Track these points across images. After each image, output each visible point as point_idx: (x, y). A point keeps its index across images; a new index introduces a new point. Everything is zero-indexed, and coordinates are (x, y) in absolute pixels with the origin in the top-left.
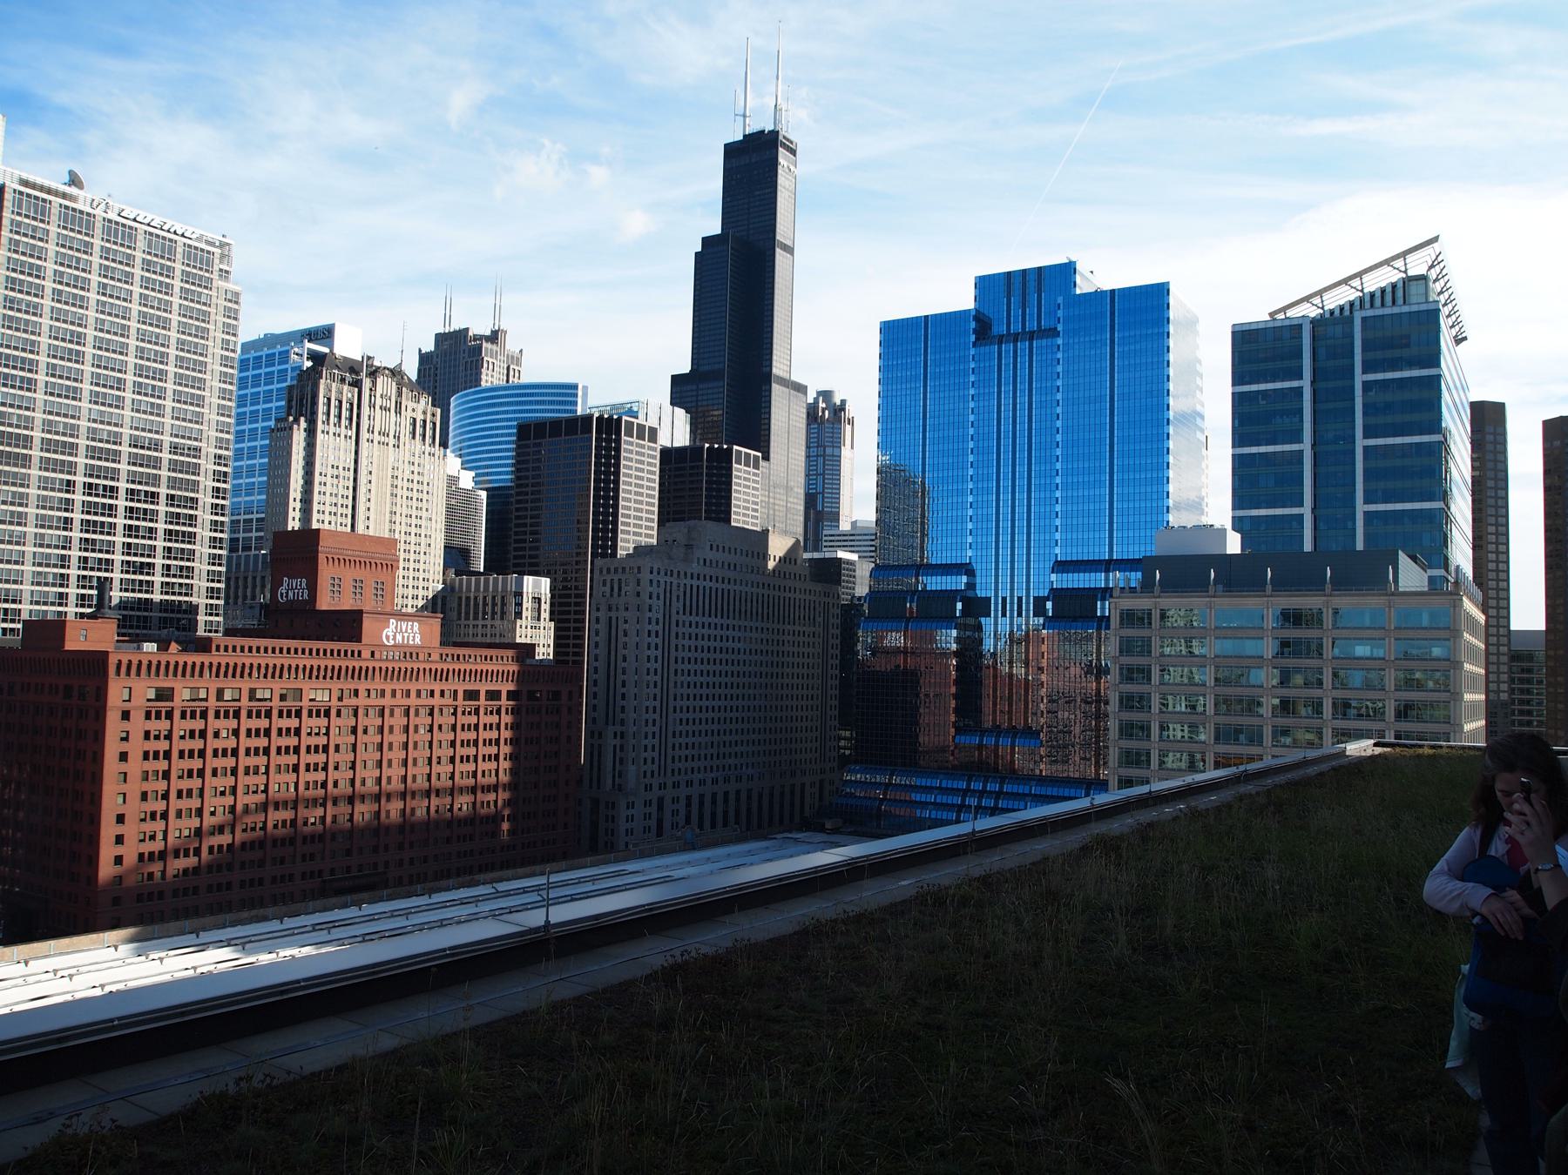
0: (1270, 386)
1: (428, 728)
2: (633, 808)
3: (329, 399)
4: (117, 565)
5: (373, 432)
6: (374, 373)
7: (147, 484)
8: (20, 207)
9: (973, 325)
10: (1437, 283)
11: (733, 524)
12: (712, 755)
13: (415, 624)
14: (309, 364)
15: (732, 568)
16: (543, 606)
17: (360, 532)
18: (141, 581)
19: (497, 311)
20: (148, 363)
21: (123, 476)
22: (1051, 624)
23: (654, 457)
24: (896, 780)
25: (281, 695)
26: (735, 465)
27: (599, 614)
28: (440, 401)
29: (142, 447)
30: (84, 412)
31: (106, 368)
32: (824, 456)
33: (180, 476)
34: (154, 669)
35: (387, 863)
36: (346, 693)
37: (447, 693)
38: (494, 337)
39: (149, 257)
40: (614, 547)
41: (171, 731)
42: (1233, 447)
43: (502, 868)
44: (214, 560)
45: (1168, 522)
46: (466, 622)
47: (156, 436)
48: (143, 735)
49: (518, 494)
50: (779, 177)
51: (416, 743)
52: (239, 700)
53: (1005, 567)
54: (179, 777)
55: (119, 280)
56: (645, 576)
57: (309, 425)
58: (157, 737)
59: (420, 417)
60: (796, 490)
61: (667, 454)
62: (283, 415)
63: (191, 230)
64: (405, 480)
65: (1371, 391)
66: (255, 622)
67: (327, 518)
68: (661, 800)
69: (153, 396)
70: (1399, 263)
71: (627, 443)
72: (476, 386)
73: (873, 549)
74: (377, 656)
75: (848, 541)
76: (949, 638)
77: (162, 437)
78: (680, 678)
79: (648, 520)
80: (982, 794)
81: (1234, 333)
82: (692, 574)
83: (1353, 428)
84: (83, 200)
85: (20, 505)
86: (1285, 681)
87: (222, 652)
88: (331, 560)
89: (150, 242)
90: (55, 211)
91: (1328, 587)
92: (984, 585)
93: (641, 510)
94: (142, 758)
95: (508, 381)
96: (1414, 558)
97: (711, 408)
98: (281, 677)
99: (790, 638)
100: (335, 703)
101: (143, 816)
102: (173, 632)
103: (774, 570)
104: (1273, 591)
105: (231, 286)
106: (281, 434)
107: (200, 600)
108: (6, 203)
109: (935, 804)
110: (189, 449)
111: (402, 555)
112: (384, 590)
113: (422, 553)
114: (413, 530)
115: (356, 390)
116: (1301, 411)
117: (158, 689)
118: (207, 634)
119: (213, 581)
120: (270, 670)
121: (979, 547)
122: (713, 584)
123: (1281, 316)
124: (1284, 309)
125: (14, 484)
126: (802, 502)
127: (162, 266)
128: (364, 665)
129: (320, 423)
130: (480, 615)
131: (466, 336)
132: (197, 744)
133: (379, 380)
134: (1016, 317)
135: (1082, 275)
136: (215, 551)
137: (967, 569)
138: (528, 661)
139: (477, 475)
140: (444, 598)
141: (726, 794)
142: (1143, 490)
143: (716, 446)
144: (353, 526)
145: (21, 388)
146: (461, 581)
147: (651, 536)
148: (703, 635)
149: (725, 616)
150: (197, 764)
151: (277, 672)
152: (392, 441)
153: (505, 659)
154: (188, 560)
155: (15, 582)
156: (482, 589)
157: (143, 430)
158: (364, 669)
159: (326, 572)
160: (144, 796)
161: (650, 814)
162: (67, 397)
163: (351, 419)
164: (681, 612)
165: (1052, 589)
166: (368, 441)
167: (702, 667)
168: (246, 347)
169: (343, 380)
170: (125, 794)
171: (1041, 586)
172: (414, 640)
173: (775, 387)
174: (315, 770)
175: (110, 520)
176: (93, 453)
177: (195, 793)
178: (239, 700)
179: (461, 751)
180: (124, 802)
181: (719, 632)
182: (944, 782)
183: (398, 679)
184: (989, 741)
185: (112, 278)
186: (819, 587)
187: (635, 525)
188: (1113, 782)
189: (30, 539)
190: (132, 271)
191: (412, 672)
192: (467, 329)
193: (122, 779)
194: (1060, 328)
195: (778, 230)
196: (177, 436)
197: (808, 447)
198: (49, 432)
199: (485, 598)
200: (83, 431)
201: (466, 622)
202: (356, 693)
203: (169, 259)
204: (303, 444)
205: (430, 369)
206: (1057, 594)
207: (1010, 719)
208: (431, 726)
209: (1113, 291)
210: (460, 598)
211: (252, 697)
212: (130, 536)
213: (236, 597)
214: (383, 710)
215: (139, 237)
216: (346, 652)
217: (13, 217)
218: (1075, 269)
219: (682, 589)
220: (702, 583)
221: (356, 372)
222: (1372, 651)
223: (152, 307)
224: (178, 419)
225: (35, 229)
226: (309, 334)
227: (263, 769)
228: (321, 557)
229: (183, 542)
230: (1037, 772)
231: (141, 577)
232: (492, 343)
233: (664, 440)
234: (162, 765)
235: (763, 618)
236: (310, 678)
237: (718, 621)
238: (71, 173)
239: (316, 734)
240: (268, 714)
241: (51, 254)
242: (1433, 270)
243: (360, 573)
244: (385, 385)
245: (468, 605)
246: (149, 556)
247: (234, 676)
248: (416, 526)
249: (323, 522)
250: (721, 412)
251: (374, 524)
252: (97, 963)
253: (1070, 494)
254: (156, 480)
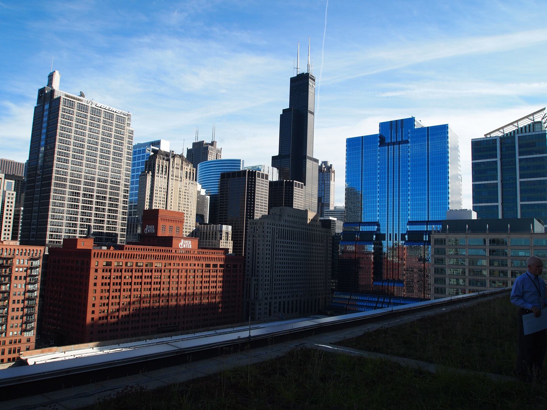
0: (486, 160)
1: (193, 277)
3: (159, 165)
6: (174, 156)
7: (103, 194)
9: (379, 139)
10: (545, 124)
11: (294, 207)
12: (288, 288)
13: (190, 241)
14: (152, 153)
17: (168, 210)
18: (100, 226)
19: (213, 135)
20: (104, 154)
22: (407, 243)
23: (267, 185)
24: (353, 297)
25: (146, 265)
26: (294, 187)
28: (195, 166)
29: (102, 182)
30: (84, 170)
31: (91, 156)
32: (324, 184)
33: (113, 191)
34: (106, 255)
35: (179, 323)
36: (167, 264)
37: (200, 265)
38: (212, 144)
39: (105, 119)
40: (253, 215)
41: (110, 276)
42: (473, 182)
43: (217, 325)
44: (123, 219)
45: (449, 208)
47: (106, 178)
48: (101, 277)
49: (221, 197)
50: (309, 89)
51: (189, 282)
52: (132, 266)
53: (391, 223)
54: (113, 292)
55: (96, 127)
56: (266, 226)
57: (152, 174)
58: (106, 278)
59: (189, 171)
60: (315, 196)
61: (271, 183)
62: (144, 170)
63: (118, 110)
64: (184, 192)
65: (522, 162)
68: (270, 303)
70: (531, 117)
71: (258, 180)
72: (206, 161)
75: (333, 213)
76: (371, 248)
78: (277, 261)
79: (265, 206)
81: (472, 142)
82: (281, 225)
83: (516, 175)
85: (63, 200)
86: (491, 263)
87: (127, 250)
88: (162, 219)
89: (106, 114)
90: (76, 105)
91: (509, 231)
92: (383, 230)
93: (262, 203)
95: (217, 159)
96: (539, 221)
97: (285, 167)
98: (146, 259)
99: (315, 247)
100: (163, 267)
103: (309, 224)
104: (489, 232)
105: (130, 128)
106: (143, 177)
107: (119, 232)
108: (61, 102)
110: (116, 182)
113: (189, 217)
116: (496, 169)
117: (107, 262)
118: (121, 244)
119: (123, 226)
120: (143, 256)
123: (489, 136)
124: (490, 133)
125: (61, 194)
127: (109, 122)
128: (173, 255)
129: (156, 173)
130: (208, 238)
131: (203, 143)
132: (119, 281)
133: (176, 159)
134: (394, 136)
135: (417, 122)
136: (124, 216)
137: (377, 224)
139: (206, 190)
140: (196, 232)
141: (293, 301)
143: (288, 181)
145: (64, 162)
146: (201, 226)
147: (266, 212)
151: (144, 257)
152: (179, 179)
154: (115, 219)
155: (60, 226)
159: (161, 224)
160: (101, 298)
162: (78, 165)
163: (166, 172)
164: (278, 238)
165: (407, 231)
166: (172, 179)
167: (285, 257)
168: (135, 147)
169: (164, 159)
170: (95, 297)
172: (189, 247)
174: (156, 290)
175: (91, 205)
176: (86, 184)
177: (118, 297)
178: (132, 266)
179: (204, 285)
180: (95, 299)
181: (290, 245)
184: (385, 284)
185: (93, 126)
186: (324, 230)
189: (65, 211)
190: (100, 124)
192: (203, 141)
197: (319, 181)
199: (209, 232)
200: (83, 176)
202: (170, 264)
203: (111, 120)
204: (150, 180)
206: (409, 233)
208: (194, 276)
209: (428, 127)
210: (201, 232)
211: (137, 265)
212: (97, 211)
213: (130, 231)
214: (179, 270)
215: (102, 113)
216: (167, 250)
219: (278, 230)
220: (285, 228)
221: (168, 156)
222: (525, 254)
224: (113, 172)
225: (70, 111)
226: (152, 143)
227: (139, 290)
229: (114, 213)
230: (403, 296)
231: (100, 225)
232: (212, 146)
233: (270, 179)
236: (155, 259)
237: (290, 241)
238: (81, 92)
239: (157, 278)
240: (142, 271)
241: (74, 119)
242: (543, 120)
243: (172, 224)
244: (177, 160)
245: (204, 235)
246: (103, 218)
248: (187, 208)
249: (156, 206)
250: (289, 169)
251: (173, 207)
252: (87, 353)
253: (413, 198)
254: (105, 192)
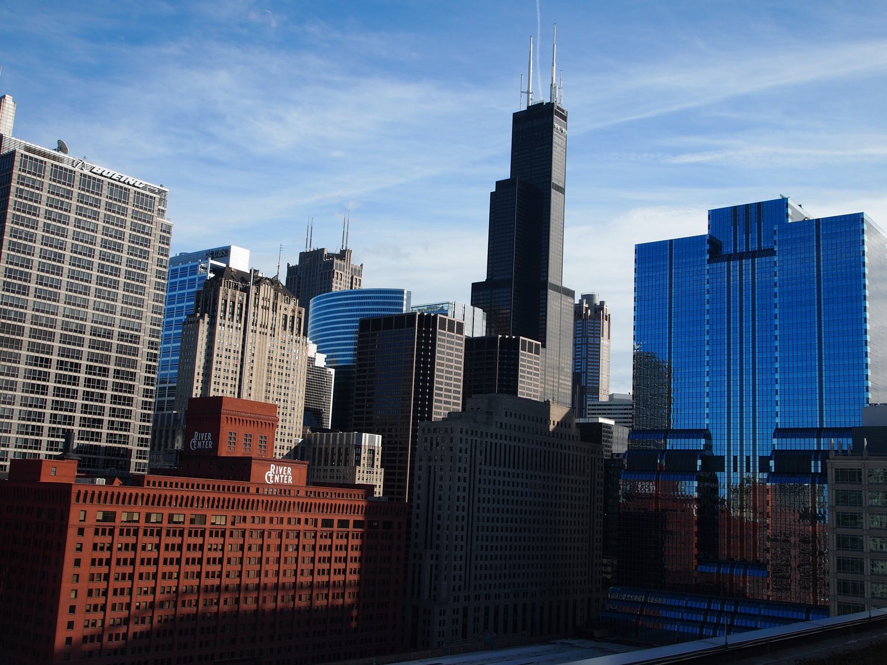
2: (444, 614)
3: (226, 301)
4: (77, 420)
5: (256, 325)
6: (259, 282)
8: (25, 166)
9: (707, 247)
11: (519, 396)
14: (212, 275)
15: (522, 430)
16: (376, 456)
17: (244, 398)
19: (345, 237)
20: (106, 276)
21: (85, 356)
23: (460, 345)
24: (651, 600)
25: (191, 519)
26: (521, 351)
27: (422, 463)
28: (304, 304)
30: (61, 310)
31: (77, 279)
33: (124, 356)
34: (103, 498)
36: (237, 519)
37: (310, 521)
38: (343, 255)
41: (112, 544)
44: (144, 418)
45: (868, 399)
46: (318, 467)
47: (109, 328)
48: (91, 546)
49: (359, 371)
52: (161, 522)
54: (116, 579)
57: (211, 320)
58: (102, 549)
59: (290, 314)
62: (192, 312)
63: (139, 181)
66: (172, 465)
67: (221, 388)
68: (465, 609)
69: (108, 299)
71: (440, 334)
73: (631, 416)
74: (261, 492)
75: (613, 407)
76: (691, 488)
77: (113, 328)
80: (720, 613)
82: (492, 434)
84: (67, 160)
85: (13, 376)
87: (151, 486)
88: (230, 420)
90: (48, 169)
93: (450, 385)
94: (90, 563)
95: (351, 288)
98: (191, 506)
100: (229, 526)
101: (88, 607)
102: (114, 470)
105: (165, 221)
106: (191, 326)
107: (134, 447)
108: (16, 164)
109: (682, 620)
111: (281, 417)
112: (267, 442)
113: (288, 415)
114: (283, 397)
115: (245, 294)
119: (143, 433)
120: (185, 500)
121: (715, 417)
122: (507, 442)
125: (10, 361)
126: (570, 379)
129: (219, 318)
130: (329, 462)
132: (130, 555)
133: (262, 288)
135: (793, 208)
137: (705, 434)
138: (370, 498)
139: (328, 357)
141: (515, 606)
142: (851, 373)
143: (507, 337)
144: (239, 394)
145: (18, 293)
146: (316, 436)
147: (458, 404)
148: (499, 481)
149: (516, 467)
150: (128, 569)
151: (188, 502)
152: (269, 332)
153: (353, 496)
154: (127, 418)
156: (331, 443)
157: (101, 323)
158: (251, 501)
159: (226, 429)
160: (90, 592)
161: (457, 620)
162: (49, 299)
164: (483, 463)
166: (252, 331)
168: (174, 261)
169: (236, 287)
170: (76, 591)
171: (765, 448)
172: (287, 480)
173: (550, 292)
174: (212, 577)
177: (126, 591)
178: (161, 522)
180: (76, 597)
182: (689, 602)
183: (275, 510)
184: (725, 570)
187: (446, 396)
188: (834, 608)
191: (285, 504)
192: (323, 250)
193: (76, 578)
194: (776, 249)
195: (553, 175)
196: (123, 327)
197: (575, 337)
198: (36, 324)
199: (333, 449)
201: (318, 467)
202: (245, 519)
203: (124, 202)
204: (206, 333)
205: (295, 278)
206: (777, 454)
207: (742, 554)
208: (298, 546)
209: (818, 220)
210: (315, 449)
212: (87, 399)
213: (160, 445)
214: (263, 532)
216: (239, 488)
217: (20, 173)
218: (787, 204)
219: (484, 445)
223: (111, 236)
225: (34, 181)
226: (212, 254)
227: (175, 575)
228: (223, 417)
229: (124, 404)
232: (341, 259)
233: (467, 332)
234: (104, 570)
235: (544, 469)
236: (212, 507)
238: (59, 142)
240: (181, 534)
241: (44, 199)
243: (250, 429)
244: (266, 291)
245: (320, 454)
247: (153, 504)
250: (509, 311)
251: (254, 392)
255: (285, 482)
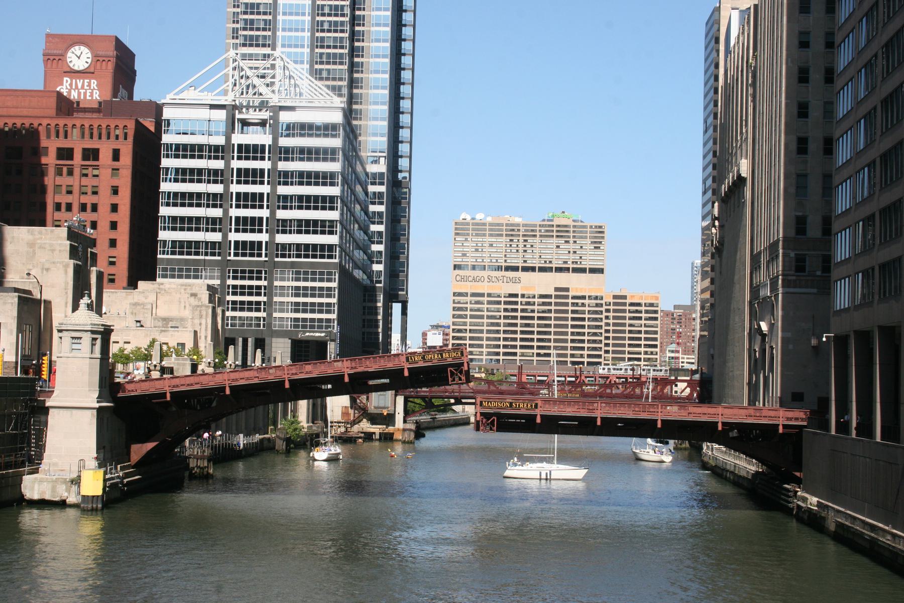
255: (88, 98)
